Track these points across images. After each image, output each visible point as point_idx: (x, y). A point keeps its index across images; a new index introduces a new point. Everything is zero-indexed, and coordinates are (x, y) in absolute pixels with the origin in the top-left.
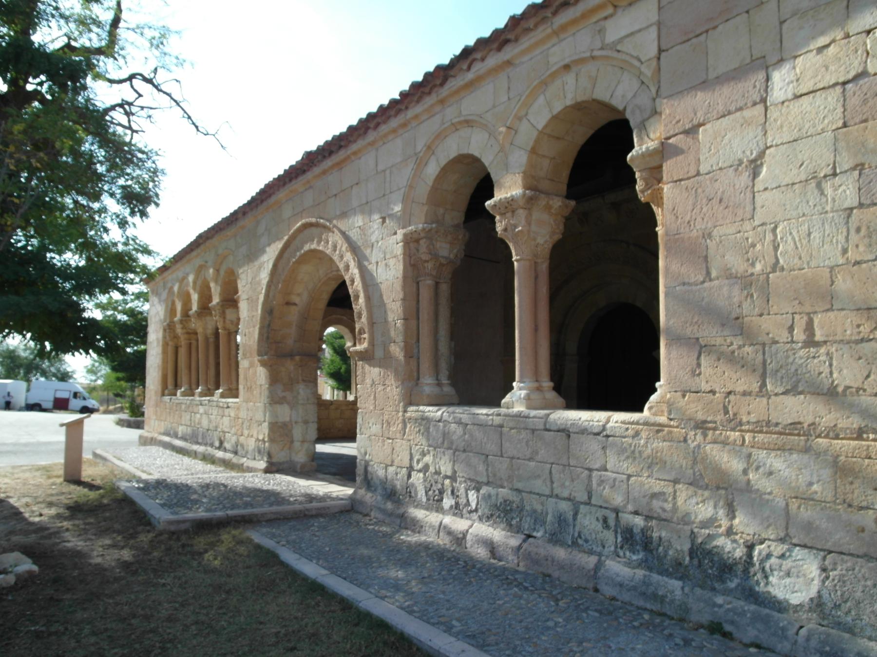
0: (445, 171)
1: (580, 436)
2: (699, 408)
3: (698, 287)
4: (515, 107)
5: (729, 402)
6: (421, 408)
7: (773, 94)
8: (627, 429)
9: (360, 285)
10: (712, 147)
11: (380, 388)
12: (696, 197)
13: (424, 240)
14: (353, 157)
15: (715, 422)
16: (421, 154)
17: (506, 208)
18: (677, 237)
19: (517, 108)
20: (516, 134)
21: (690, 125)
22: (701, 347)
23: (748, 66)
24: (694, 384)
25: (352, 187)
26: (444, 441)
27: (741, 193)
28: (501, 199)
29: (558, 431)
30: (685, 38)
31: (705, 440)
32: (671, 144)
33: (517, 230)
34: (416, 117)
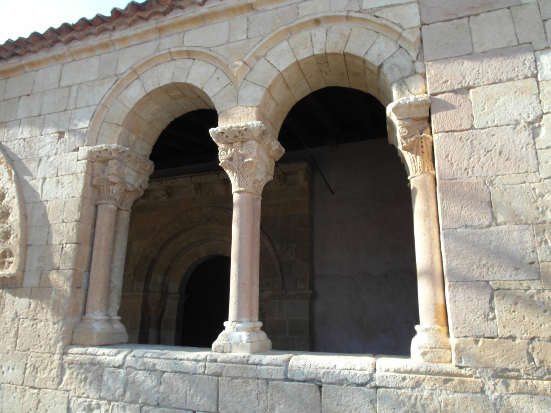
0: (150, 96)
1: (338, 387)
2: (498, 354)
3: (483, 230)
4: (254, 47)
5: (533, 348)
6: (91, 350)
7: (543, 72)
8: (404, 379)
9: (16, 201)
10: (486, 107)
11: (27, 323)
12: (472, 147)
13: (116, 161)
14: (27, 69)
15: (518, 371)
16: (124, 76)
17: (236, 137)
18: (453, 181)
19: (257, 47)
20: (251, 70)
21: (459, 86)
22: (493, 291)
23: (515, 48)
24: (488, 329)
25: (20, 97)
26: (125, 392)
27: (522, 148)
28: (231, 127)
29: (304, 381)
30: (448, 18)
31: (507, 391)
32: (439, 100)
33: (245, 161)
34: (124, 39)
